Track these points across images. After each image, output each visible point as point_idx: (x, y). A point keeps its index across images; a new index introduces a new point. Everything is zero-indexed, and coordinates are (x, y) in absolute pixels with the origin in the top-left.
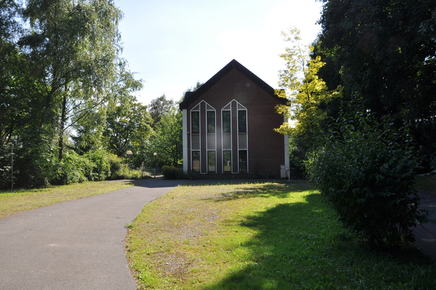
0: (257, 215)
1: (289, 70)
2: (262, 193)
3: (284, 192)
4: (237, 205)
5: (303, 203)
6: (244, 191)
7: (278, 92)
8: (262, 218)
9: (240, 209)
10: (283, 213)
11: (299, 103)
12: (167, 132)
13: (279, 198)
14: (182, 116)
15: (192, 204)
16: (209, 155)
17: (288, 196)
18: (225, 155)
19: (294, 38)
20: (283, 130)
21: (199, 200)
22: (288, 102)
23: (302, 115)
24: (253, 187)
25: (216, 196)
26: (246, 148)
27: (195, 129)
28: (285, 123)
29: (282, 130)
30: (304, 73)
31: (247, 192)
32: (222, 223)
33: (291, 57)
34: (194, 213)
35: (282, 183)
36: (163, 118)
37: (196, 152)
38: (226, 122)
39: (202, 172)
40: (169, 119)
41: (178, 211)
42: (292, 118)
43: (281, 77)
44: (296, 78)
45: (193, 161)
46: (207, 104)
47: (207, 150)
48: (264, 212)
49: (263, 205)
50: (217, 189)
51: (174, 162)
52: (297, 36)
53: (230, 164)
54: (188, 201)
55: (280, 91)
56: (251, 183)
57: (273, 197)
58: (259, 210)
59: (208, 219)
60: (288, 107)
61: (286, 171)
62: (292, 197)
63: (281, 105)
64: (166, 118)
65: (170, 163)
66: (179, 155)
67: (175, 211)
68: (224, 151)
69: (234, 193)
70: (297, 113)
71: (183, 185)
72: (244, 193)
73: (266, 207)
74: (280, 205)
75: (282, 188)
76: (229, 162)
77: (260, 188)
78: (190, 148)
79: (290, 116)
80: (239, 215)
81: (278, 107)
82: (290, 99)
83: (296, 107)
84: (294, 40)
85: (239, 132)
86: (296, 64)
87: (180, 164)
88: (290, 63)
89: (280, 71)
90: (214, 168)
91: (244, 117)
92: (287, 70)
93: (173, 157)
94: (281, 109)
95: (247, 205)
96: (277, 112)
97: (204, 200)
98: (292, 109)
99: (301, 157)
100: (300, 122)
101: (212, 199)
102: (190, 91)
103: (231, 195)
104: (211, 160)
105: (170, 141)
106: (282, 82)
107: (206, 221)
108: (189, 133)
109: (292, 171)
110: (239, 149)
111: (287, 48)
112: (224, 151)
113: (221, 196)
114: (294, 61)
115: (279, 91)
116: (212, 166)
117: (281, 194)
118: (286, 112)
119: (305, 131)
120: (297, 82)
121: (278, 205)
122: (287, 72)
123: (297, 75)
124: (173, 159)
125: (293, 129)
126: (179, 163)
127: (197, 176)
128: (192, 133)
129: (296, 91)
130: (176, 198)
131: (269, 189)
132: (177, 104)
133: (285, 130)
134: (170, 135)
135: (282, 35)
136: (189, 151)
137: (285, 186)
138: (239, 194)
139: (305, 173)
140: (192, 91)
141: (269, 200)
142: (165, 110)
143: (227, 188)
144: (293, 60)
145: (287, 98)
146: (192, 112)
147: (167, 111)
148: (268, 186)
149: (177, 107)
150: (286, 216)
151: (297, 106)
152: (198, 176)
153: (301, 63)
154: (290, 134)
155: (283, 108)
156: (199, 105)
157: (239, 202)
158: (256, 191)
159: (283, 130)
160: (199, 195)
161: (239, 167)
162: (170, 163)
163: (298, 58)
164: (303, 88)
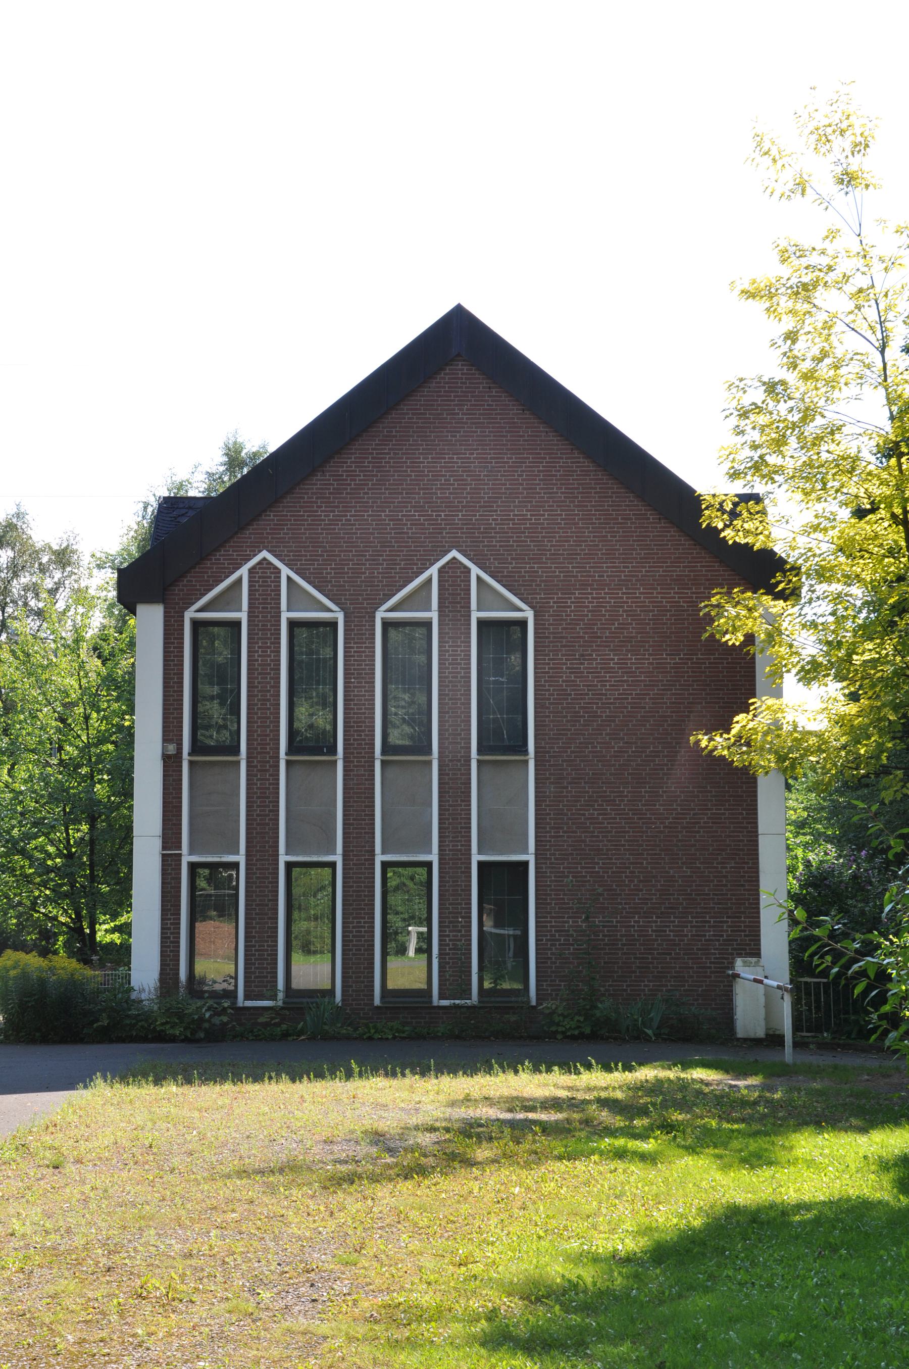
0: (587, 1275)
1: (792, 378)
2: (617, 1130)
3: (756, 1127)
4: (464, 1208)
5: (880, 1202)
6: (508, 1116)
7: (721, 509)
8: (616, 1298)
9: (480, 1231)
10: (754, 1264)
11: (849, 579)
12: (32, 742)
13: (725, 1168)
14: (132, 644)
15: (178, 1200)
16: (296, 891)
17: (782, 1155)
18: (397, 888)
19: (831, 181)
20: (748, 744)
21: (228, 1176)
22: (784, 572)
23: (867, 652)
24: (563, 1094)
25: (336, 1148)
26: (525, 851)
27: (207, 727)
28: (763, 703)
29: (745, 741)
30: (888, 394)
31: (528, 1124)
32: (369, 1326)
33: (808, 300)
34: (193, 1262)
35: (742, 1073)
36: (13, 652)
37: (214, 867)
38: (405, 691)
39: (247, 997)
40: (51, 663)
41: (85, 1249)
42: (808, 672)
43: (743, 423)
44: (834, 430)
45: (197, 924)
46: (289, 578)
47: (283, 859)
48: (628, 1260)
49: (624, 1209)
50: (338, 1101)
51: (75, 931)
52: (852, 168)
53: (424, 949)
54: (152, 1184)
55: (735, 505)
56: (549, 1070)
57: (689, 1160)
58: (603, 1244)
59: (282, 1304)
60: (781, 603)
61: (767, 995)
62: (810, 1163)
63: (743, 592)
64: (28, 655)
65: (47, 936)
66: (105, 888)
67: (69, 1252)
68: (385, 865)
69: (447, 1130)
70: (840, 643)
71: (124, 1079)
72: (507, 1130)
73: (647, 1221)
74: (734, 1211)
75: (744, 1103)
76: (420, 934)
77: (605, 1103)
78: (180, 848)
79: (795, 659)
80: (475, 1277)
81: (718, 606)
82: (796, 553)
83: (830, 609)
84: (829, 187)
85: (480, 751)
86: (836, 343)
87: (112, 943)
88: (802, 338)
89: (738, 385)
90: (327, 968)
91: (515, 658)
92: (783, 383)
93: (66, 895)
94: (738, 615)
95: (524, 1208)
96: (712, 636)
97: (261, 1172)
98: (809, 618)
99: (863, 913)
100: (854, 697)
101: (309, 1169)
102: (182, 493)
103: (426, 1139)
104: (308, 919)
105: (53, 799)
106: (747, 452)
107: (264, 1315)
108: (172, 749)
109: (808, 994)
110: (480, 852)
111: (783, 244)
112: (385, 865)
113: (364, 1149)
114: (827, 326)
115: (728, 506)
116: (312, 959)
117: (736, 1144)
118: (769, 636)
119: (887, 750)
120: (838, 450)
121: (719, 1211)
122: (780, 388)
123: (841, 407)
124: (65, 911)
125: (813, 740)
126: (108, 938)
127: (216, 1020)
128: (193, 751)
129: (831, 506)
130: (79, 1161)
131: (664, 1105)
132: (99, 567)
133: (764, 741)
134: (55, 761)
135: (759, 159)
136: (170, 864)
137: (765, 1087)
138: (479, 1136)
139: (881, 1017)
140: (195, 491)
141: (666, 1181)
142: (26, 604)
143: (405, 1095)
144: (822, 317)
145: (776, 549)
146: (197, 625)
147: (39, 613)
148: (656, 1088)
149: (100, 588)
150: (770, 1285)
151: (838, 598)
152: (225, 1019)
153: (873, 339)
154: (793, 767)
155: (750, 610)
156: (239, 581)
157: (475, 1186)
158: (581, 1122)
159: (748, 744)
160: (224, 1144)
161: (481, 968)
162: (47, 936)
163: (851, 306)
164: (877, 491)
